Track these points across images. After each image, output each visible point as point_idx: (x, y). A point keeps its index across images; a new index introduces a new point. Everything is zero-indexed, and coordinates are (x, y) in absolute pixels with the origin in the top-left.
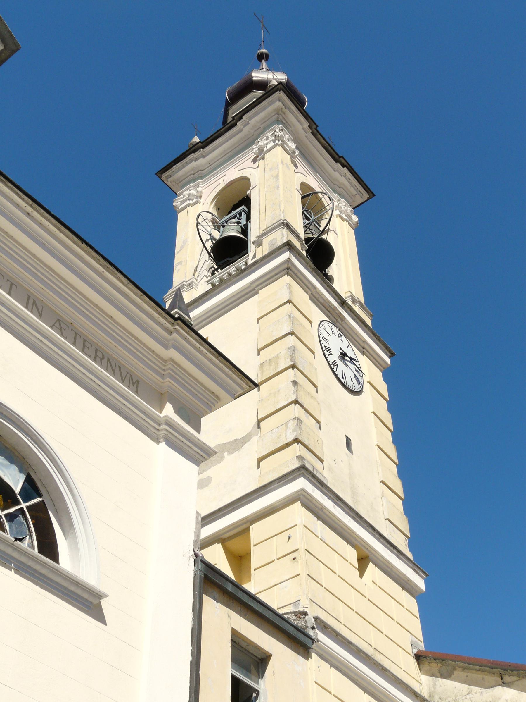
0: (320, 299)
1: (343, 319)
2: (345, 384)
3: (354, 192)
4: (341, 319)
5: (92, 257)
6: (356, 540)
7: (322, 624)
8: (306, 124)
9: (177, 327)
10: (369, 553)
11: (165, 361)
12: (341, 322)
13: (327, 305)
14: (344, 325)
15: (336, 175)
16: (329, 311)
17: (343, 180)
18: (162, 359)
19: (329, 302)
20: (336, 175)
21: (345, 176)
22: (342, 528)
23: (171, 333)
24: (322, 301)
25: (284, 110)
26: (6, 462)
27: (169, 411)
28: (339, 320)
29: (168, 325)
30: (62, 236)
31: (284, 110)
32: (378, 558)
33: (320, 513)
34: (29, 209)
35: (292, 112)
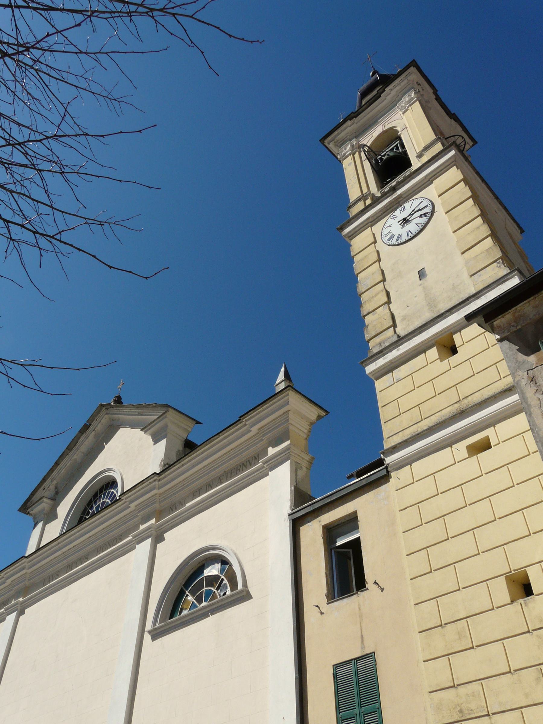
0: (378, 215)
1: (400, 196)
2: (423, 225)
3: (406, 81)
4: (399, 198)
5: (205, 446)
6: (430, 341)
7: (390, 450)
8: (349, 123)
9: (244, 420)
10: (450, 332)
11: (258, 433)
12: (401, 199)
13: (384, 210)
14: (405, 196)
15: (389, 98)
16: (390, 208)
17: (393, 93)
18: (256, 434)
19: (384, 207)
20: (389, 98)
21: (391, 90)
22: (414, 350)
23: (246, 425)
24: (381, 213)
25: (336, 140)
26: (213, 566)
27: (272, 451)
28: (400, 200)
29: (241, 424)
30: (192, 456)
31: (336, 140)
32: (458, 325)
33: (393, 365)
34: (181, 464)
35: (336, 136)
